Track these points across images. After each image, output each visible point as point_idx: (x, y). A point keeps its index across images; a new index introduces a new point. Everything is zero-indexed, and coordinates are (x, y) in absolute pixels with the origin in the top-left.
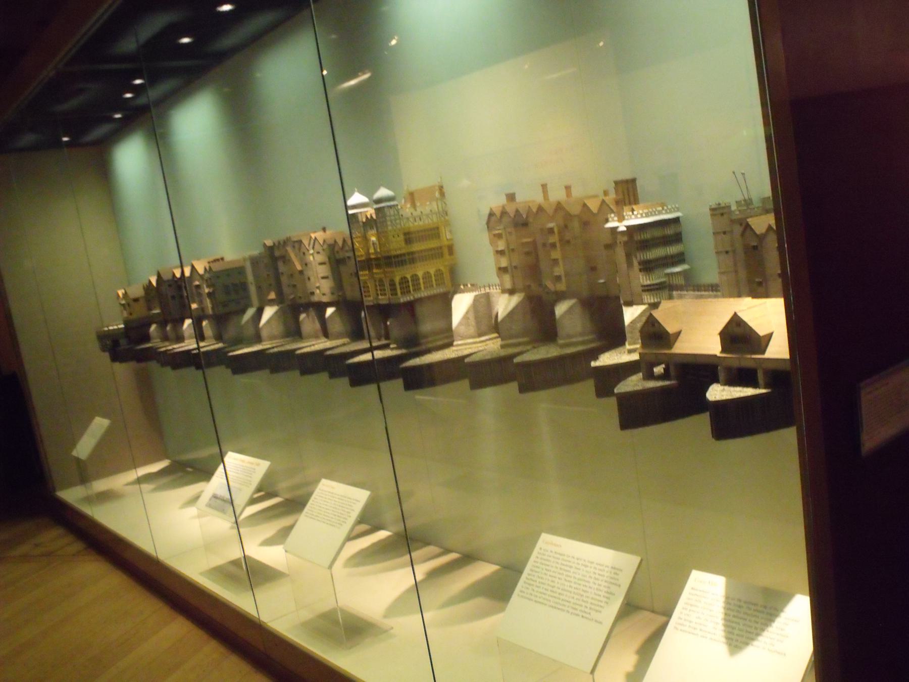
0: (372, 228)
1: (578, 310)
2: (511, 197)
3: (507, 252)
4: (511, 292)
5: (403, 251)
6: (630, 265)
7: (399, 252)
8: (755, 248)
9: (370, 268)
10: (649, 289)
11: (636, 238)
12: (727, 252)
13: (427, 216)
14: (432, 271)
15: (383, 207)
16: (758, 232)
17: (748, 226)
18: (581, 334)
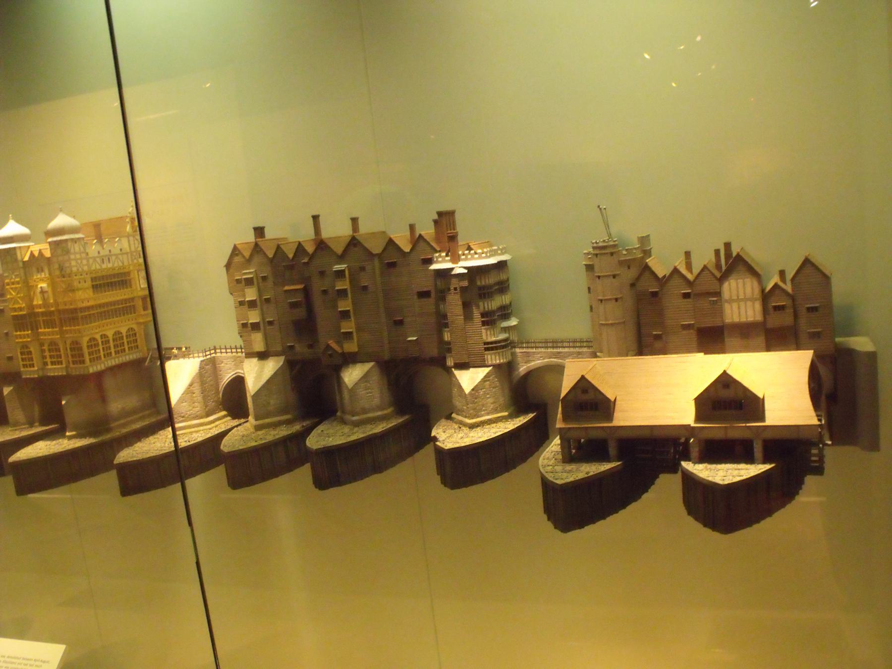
0: (40, 270)
1: (376, 377)
2: (259, 231)
3: (258, 303)
4: (263, 356)
5: (91, 303)
6: (468, 317)
7: (86, 304)
8: (654, 294)
9: (34, 327)
10: (491, 347)
11: (479, 283)
12: (616, 300)
13: (116, 255)
14: (124, 331)
15: (66, 240)
16: (660, 275)
17: (647, 268)
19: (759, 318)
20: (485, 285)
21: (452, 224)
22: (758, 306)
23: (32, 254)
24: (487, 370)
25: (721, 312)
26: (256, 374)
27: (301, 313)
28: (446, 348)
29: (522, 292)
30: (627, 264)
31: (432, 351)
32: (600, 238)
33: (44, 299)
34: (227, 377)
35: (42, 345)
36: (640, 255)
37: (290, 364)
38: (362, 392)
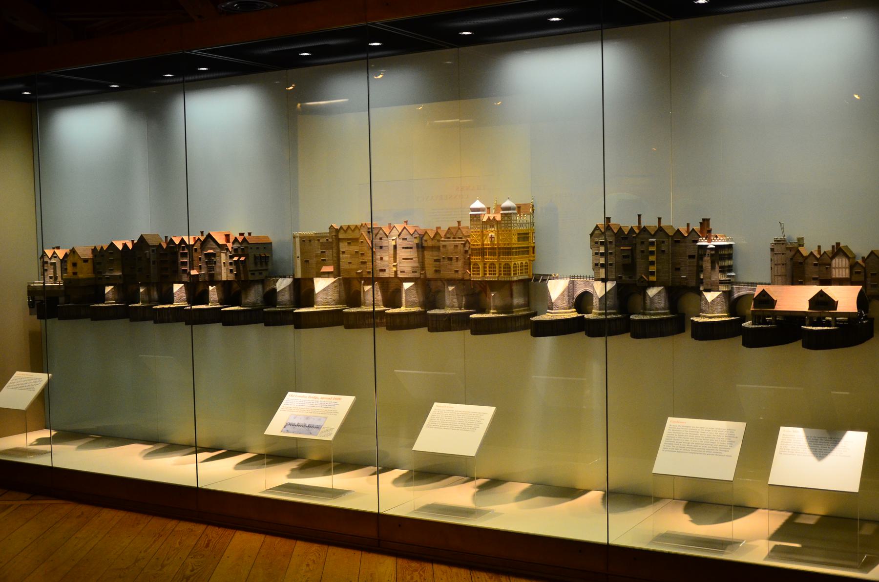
6: (713, 268)
8: (801, 263)
10: (722, 282)
17: (798, 251)
18: (664, 309)
19: (848, 276)
20: (723, 254)
21: (708, 225)
22: (848, 271)
23: (489, 218)
24: (718, 293)
25: (831, 272)
26: (599, 289)
27: (628, 261)
28: (701, 282)
29: (739, 261)
30: (790, 249)
31: (693, 283)
32: (780, 236)
33: (492, 241)
34: (579, 291)
35: (485, 264)
36: (796, 245)
37: (617, 284)
38: (656, 300)
